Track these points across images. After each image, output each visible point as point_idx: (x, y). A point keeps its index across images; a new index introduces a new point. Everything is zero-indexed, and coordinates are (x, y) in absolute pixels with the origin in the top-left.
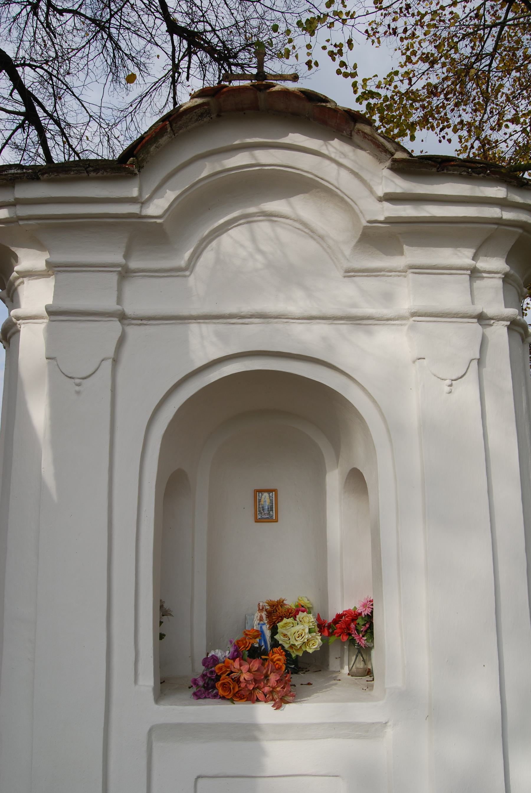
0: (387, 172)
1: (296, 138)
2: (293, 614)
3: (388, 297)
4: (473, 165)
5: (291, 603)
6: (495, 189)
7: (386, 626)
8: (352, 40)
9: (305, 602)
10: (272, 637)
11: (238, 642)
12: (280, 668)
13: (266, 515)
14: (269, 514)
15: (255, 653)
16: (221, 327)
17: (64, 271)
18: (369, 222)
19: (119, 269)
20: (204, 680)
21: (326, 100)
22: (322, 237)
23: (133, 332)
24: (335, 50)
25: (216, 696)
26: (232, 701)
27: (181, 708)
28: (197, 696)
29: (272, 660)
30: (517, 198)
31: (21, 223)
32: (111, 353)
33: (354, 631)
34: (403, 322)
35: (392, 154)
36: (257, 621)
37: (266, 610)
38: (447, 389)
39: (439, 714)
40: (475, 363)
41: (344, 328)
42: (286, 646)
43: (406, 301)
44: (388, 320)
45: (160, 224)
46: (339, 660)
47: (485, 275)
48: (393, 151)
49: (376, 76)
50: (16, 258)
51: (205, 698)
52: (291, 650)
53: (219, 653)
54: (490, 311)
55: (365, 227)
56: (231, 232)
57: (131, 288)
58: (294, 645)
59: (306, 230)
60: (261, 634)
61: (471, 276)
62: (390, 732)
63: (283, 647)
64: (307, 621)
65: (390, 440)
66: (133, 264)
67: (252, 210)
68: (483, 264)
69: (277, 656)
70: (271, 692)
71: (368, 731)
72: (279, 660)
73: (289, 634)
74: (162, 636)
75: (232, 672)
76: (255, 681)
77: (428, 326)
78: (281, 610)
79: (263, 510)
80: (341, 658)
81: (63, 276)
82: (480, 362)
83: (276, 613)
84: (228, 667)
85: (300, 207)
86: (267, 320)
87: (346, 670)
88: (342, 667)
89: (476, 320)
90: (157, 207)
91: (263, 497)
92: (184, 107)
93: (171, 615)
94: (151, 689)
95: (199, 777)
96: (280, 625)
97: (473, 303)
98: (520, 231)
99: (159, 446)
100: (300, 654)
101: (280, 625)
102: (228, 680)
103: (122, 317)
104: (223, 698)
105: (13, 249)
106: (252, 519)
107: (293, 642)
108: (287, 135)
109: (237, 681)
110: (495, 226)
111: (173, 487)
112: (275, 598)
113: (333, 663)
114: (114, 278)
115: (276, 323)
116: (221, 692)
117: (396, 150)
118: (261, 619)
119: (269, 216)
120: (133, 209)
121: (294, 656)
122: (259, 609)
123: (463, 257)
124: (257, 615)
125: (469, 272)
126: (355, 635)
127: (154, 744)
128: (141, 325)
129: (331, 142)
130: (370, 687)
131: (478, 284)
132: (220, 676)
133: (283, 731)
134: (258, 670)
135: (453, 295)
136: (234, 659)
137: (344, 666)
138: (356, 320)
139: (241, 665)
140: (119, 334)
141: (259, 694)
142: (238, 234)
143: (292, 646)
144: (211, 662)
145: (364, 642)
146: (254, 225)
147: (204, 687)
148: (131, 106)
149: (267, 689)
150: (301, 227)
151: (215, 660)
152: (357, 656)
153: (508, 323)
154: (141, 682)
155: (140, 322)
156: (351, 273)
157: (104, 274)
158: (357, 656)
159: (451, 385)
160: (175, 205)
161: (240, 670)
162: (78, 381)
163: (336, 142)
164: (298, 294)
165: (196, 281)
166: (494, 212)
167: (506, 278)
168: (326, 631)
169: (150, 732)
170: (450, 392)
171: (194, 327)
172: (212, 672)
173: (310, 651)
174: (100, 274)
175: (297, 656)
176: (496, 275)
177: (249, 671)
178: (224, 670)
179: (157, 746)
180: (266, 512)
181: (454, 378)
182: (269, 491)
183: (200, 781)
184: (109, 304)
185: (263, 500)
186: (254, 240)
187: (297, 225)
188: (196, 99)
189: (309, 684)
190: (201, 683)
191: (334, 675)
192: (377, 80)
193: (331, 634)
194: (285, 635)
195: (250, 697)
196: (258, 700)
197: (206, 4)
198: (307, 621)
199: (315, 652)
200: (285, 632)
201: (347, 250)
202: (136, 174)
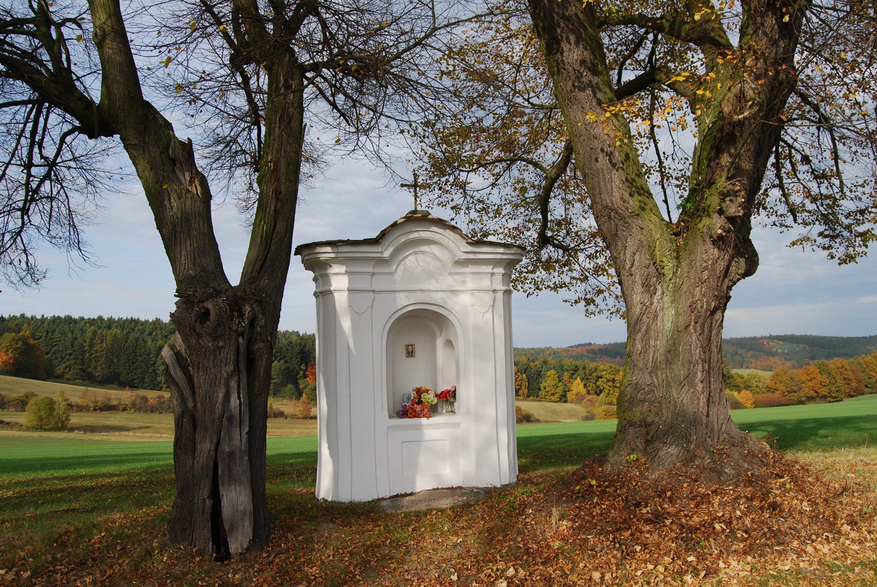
3: (464, 282)
7: (461, 394)
13: (410, 354)
16: (407, 294)
23: (377, 296)
33: (448, 397)
39: (478, 418)
41: (449, 294)
43: (470, 285)
57: (375, 278)
62: (462, 425)
66: (376, 271)
67: (417, 250)
68: (495, 271)
71: (456, 425)
77: (476, 294)
83: (419, 392)
85: (434, 249)
90: (386, 254)
103: (374, 291)
106: (404, 353)
113: (440, 409)
119: (422, 252)
131: (494, 277)
133: (430, 426)
135: (486, 283)
137: (446, 408)
138: (453, 292)
142: (411, 258)
156: (450, 274)
164: (433, 281)
165: (398, 275)
166: (499, 256)
171: (397, 294)
184: (367, 286)
186: (417, 261)
195: (419, 417)
201: (450, 265)
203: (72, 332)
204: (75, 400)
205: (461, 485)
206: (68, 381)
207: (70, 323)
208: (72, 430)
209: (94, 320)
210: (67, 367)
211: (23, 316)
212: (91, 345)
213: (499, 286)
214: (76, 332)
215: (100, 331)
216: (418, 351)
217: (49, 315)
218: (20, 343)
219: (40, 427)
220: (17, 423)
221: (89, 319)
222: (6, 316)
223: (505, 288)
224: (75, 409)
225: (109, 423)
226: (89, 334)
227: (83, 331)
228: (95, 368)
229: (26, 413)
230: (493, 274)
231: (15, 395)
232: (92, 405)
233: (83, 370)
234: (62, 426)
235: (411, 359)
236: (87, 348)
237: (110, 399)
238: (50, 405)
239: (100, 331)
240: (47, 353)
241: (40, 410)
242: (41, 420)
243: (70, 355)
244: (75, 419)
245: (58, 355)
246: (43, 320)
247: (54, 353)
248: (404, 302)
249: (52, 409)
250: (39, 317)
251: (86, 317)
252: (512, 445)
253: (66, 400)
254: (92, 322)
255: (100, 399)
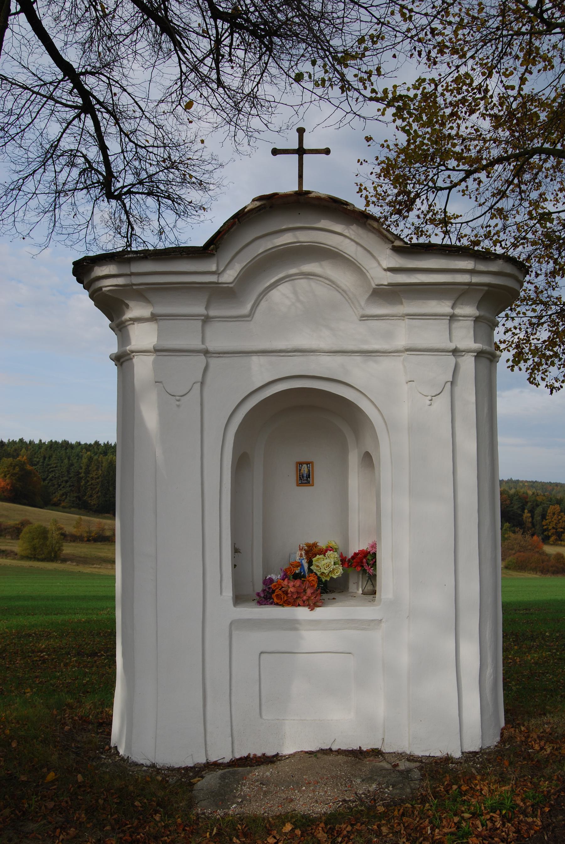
0: (389, 252)
1: (324, 223)
2: (323, 552)
4: (449, 249)
5: (322, 545)
6: (467, 262)
8: (380, 68)
9: (333, 544)
10: (309, 568)
11: (286, 569)
12: (313, 586)
13: (305, 479)
14: (307, 480)
15: (296, 576)
17: (164, 319)
18: (377, 285)
19: (203, 318)
20: (264, 593)
21: (347, 204)
22: (345, 291)
23: (214, 362)
24: (365, 76)
25: (271, 604)
26: (282, 605)
27: (250, 609)
28: (260, 603)
29: (308, 581)
30: (481, 267)
31: (134, 287)
32: (200, 379)
34: (401, 354)
35: (393, 242)
36: (298, 556)
37: (305, 550)
38: (429, 402)
40: (449, 384)
42: (319, 574)
44: (390, 352)
45: (231, 288)
46: (356, 584)
47: (461, 318)
48: (393, 240)
49: (405, 83)
50: (127, 306)
51: (265, 604)
52: (322, 577)
53: (274, 577)
54: (462, 345)
55: (374, 288)
56: (279, 287)
57: (213, 329)
58: (324, 573)
59: (333, 286)
60: (301, 565)
61: (450, 320)
63: (316, 574)
64: (332, 557)
65: (389, 437)
66: (212, 313)
68: (461, 310)
69: (312, 578)
70: (308, 600)
72: (313, 580)
73: (320, 565)
74: (235, 566)
75: (283, 587)
76: (298, 593)
78: (315, 550)
79: (303, 477)
80: (357, 583)
81: (162, 323)
82: (452, 383)
83: (312, 551)
84: (280, 585)
86: (305, 354)
87: (360, 591)
88: (358, 590)
89: (451, 354)
90: (229, 276)
91: (303, 467)
92: (248, 209)
93: (240, 552)
94: (231, 598)
95: (262, 653)
96: (314, 559)
97: (451, 340)
98: (486, 288)
99: (233, 441)
100: (328, 579)
101: (314, 559)
102: (280, 592)
103: (206, 353)
104: (277, 604)
105: (127, 302)
106: (293, 478)
107: (323, 570)
108: (319, 221)
109: (286, 593)
110: (467, 287)
111: (241, 463)
112: (311, 542)
113: (352, 587)
114: (199, 323)
115: (312, 355)
116: (275, 600)
117: (395, 239)
118: (301, 556)
120: (213, 278)
121: (323, 580)
122: (300, 549)
123: (444, 307)
124: (299, 553)
125: (449, 318)
126: (366, 567)
127: (233, 632)
128: (218, 357)
129: (352, 227)
130: (373, 600)
131: (455, 325)
132: (275, 591)
133: (316, 624)
134: (299, 586)
135: (434, 335)
136: (283, 580)
137: (357, 587)
139: (288, 583)
140: (205, 365)
141: (299, 601)
142: (284, 289)
143: (323, 573)
144: (268, 582)
145: (371, 571)
146: (296, 281)
147: (264, 597)
148: (176, 83)
149: (305, 598)
150: (330, 283)
151: (271, 580)
152: (368, 581)
153: (475, 354)
154: (224, 594)
155: (218, 355)
156: (365, 318)
157: (192, 321)
158: (368, 581)
159: (431, 400)
160: (242, 273)
161: (288, 586)
162: (178, 398)
163: (354, 227)
166: (465, 278)
167: (477, 320)
168: (346, 564)
169: (231, 624)
170: (430, 405)
171: (255, 359)
172: (269, 588)
173: (335, 577)
174: (189, 321)
175: (326, 580)
176: (469, 318)
177: (294, 586)
178: (277, 586)
179: (235, 633)
180: (305, 478)
181: (433, 395)
182: (307, 463)
183: (262, 655)
184: (196, 344)
185: (302, 469)
186: (295, 293)
187: (327, 282)
188: (256, 202)
189: (334, 599)
190: (262, 595)
191: (351, 594)
192: (406, 87)
193: (349, 566)
194: (318, 566)
196: (299, 605)
197: (248, 1)
198: (332, 557)
199: (338, 578)
200: (318, 564)
202: (214, 254)
203: (69, 458)
204: (70, 529)
205: (377, 746)
206: (64, 509)
207: (66, 449)
208: (64, 561)
209: (90, 445)
210: (63, 495)
211: (21, 440)
212: (87, 472)
213: (465, 338)
214: (72, 458)
215: (96, 457)
216: (319, 475)
217: (46, 440)
218: (17, 469)
219: (34, 555)
220: (12, 552)
221: (86, 444)
222: (6, 441)
223: (478, 346)
224: (69, 538)
225: (102, 554)
226: (85, 460)
227: (79, 457)
228: (91, 496)
229: (20, 542)
230: (452, 318)
231: (11, 523)
232: (85, 535)
233: (78, 498)
234: (54, 556)
235: (305, 490)
236: (82, 475)
237: (103, 530)
238: (43, 533)
239: (96, 457)
240: (44, 480)
241: (33, 539)
242: (35, 549)
243: (67, 482)
244: (68, 549)
245: (55, 482)
246: (41, 444)
247: (51, 480)
248: (261, 373)
249: (46, 538)
250: (37, 442)
251: (83, 443)
252: (489, 671)
253: (61, 529)
254: (88, 447)
255: (94, 529)
